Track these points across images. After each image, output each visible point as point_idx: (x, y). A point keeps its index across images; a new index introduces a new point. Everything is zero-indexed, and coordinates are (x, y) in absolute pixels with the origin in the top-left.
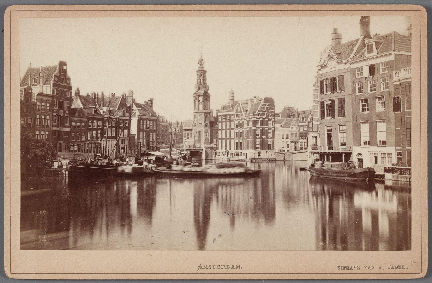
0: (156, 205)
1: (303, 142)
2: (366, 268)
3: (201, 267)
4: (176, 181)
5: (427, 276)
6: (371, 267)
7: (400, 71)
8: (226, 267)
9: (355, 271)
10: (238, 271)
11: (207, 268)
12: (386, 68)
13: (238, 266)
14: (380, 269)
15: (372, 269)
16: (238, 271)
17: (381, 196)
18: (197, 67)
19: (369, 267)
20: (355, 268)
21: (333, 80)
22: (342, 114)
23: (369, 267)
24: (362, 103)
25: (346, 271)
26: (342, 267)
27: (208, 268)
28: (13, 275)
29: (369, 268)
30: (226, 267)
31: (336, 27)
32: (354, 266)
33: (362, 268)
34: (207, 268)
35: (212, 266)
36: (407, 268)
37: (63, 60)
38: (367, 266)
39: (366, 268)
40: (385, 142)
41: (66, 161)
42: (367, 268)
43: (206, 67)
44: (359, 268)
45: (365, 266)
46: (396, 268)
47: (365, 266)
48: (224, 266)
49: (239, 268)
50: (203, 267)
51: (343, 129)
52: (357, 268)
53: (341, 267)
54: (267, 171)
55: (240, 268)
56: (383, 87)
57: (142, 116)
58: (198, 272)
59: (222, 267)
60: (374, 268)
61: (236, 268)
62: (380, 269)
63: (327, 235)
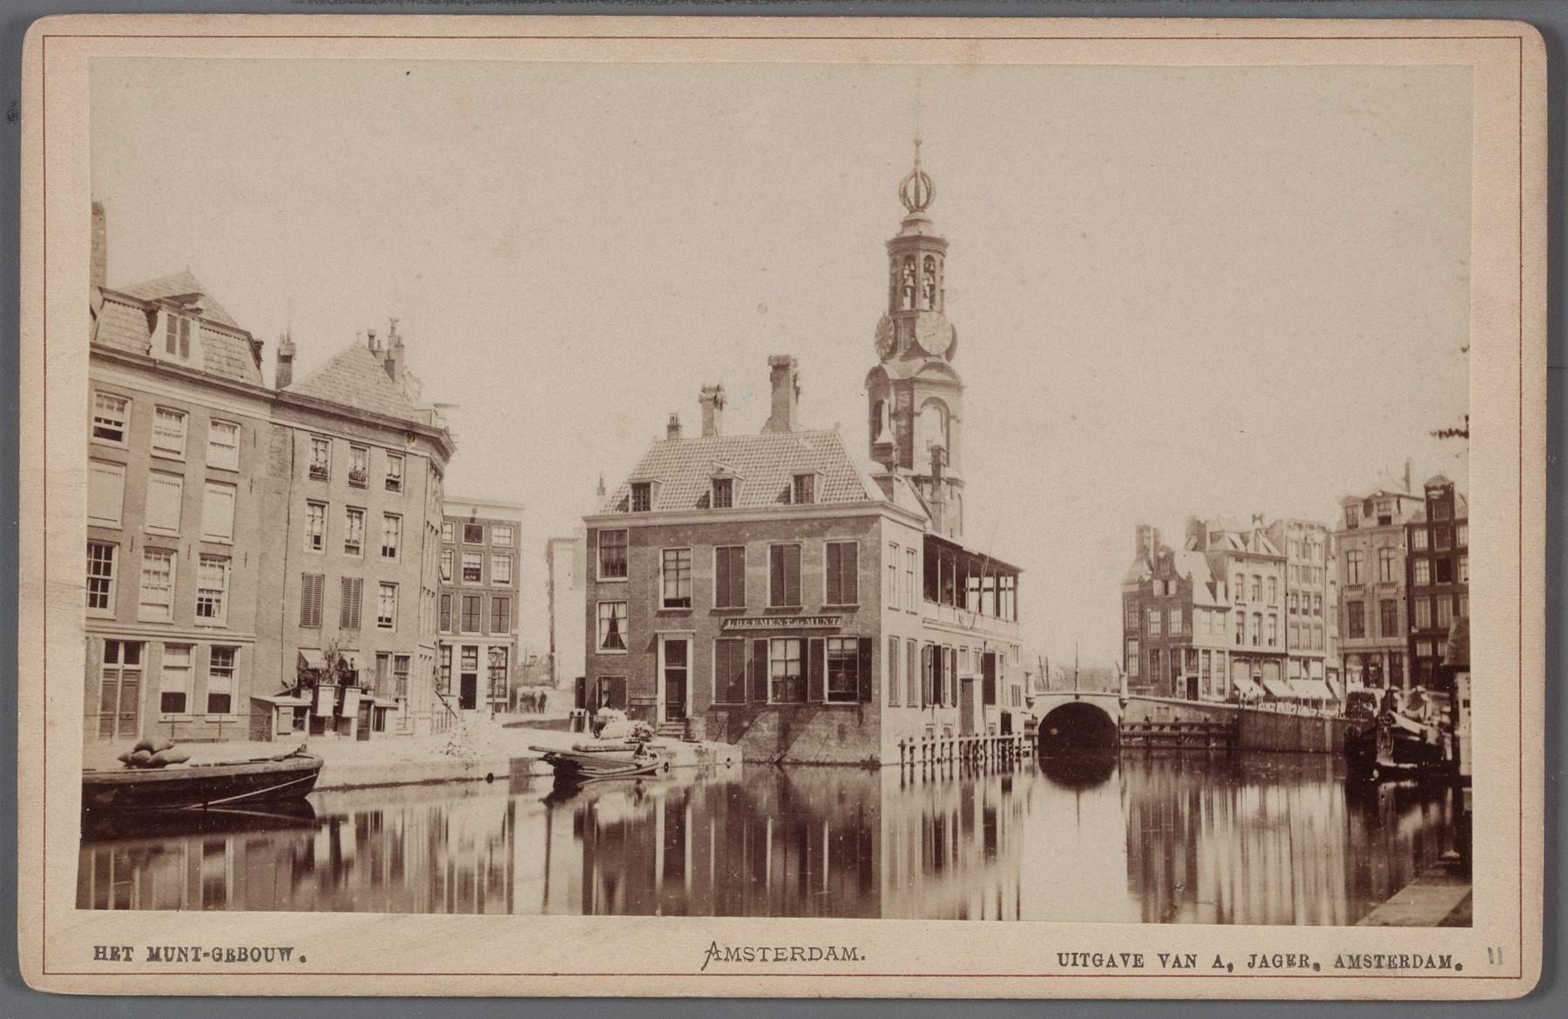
0: (1467, 598)
3: (717, 952)
6: (1183, 961)
7: (406, 367)
8: (807, 955)
11: (739, 959)
13: (849, 950)
16: (849, 967)
23: (1430, 960)
24: (106, 596)
26: (1075, 954)
30: (807, 955)
32: (1123, 955)
34: (739, 959)
35: (755, 949)
37: (778, 352)
40: (384, 554)
43: (938, 221)
45: (1161, 956)
47: (1161, 956)
48: (800, 951)
49: (855, 959)
50: (723, 955)
55: (859, 957)
56: (110, 559)
58: (704, 972)
60: (1193, 962)
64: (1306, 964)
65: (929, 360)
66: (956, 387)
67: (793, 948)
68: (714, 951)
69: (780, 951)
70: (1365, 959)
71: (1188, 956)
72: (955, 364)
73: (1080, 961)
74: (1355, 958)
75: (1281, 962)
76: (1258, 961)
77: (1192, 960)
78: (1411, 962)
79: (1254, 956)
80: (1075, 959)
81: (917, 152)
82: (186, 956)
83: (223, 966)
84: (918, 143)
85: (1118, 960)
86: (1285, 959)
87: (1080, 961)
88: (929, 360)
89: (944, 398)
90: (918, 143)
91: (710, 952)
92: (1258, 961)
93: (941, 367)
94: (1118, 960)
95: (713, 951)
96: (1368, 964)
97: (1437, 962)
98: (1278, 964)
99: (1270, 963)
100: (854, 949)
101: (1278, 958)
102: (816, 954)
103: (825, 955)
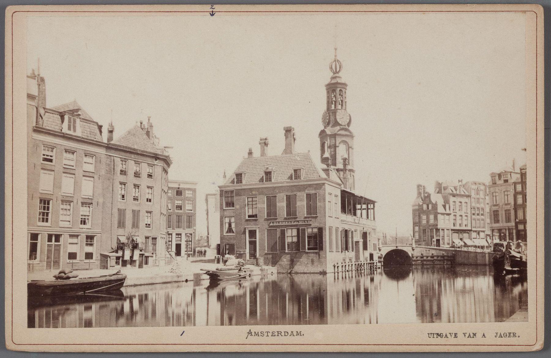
1: (40, 206)
2: (465, 336)
3: (251, 333)
4: (393, 280)
6: (472, 335)
9: (452, 340)
12: (45, 212)
18: (327, 77)
19: (470, 335)
20: (451, 336)
21: (82, 204)
22: (122, 199)
23: (470, 335)
25: (439, 340)
27: (260, 336)
31: (289, 126)
33: (460, 335)
39: (465, 336)
42: (467, 335)
43: (344, 77)
46: (505, 335)
47: (464, 334)
48: (280, 333)
50: (253, 334)
51: (519, 173)
52: (453, 335)
53: (432, 334)
55: (302, 334)
59: (278, 333)
61: (297, 335)
69: (273, 333)
71: (473, 334)
77: (475, 335)
80: (433, 335)
81: (336, 53)
84: (336, 49)
86: (508, 334)
90: (336, 49)
92: (499, 335)
93: (346, 130)
94: (449, 335)
95: (250, 333)
98: (505, 336)
100: (300, 332)
101: (505, 334)
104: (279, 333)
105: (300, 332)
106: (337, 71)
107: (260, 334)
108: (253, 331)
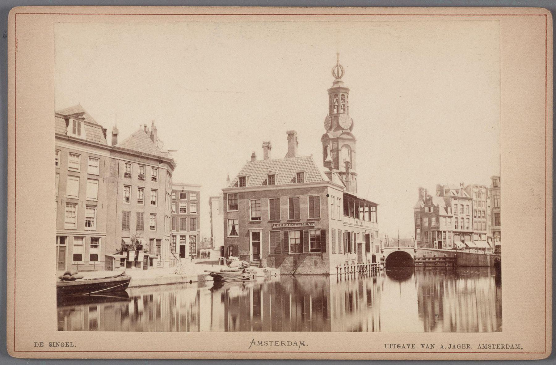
4: (395, 282)
5: (550, 358)
6: (430, 346)
8: (286, 344)
10: (303, 348)
13: (260, 343)
14: (442, 347)
15: (56, 346)
17: (251, 303)
28: (240, 354)
29: (428, 347)
30: (286, 344)
33: (46, 345)
35: (268, 341)
36: (522, 349)
38: (424, 345)
41: (447, 264)
43: (346, 82)
44: (42, 345)
48: (284, 343)
50: (257, 343)
54: (471, 279)
57: (107, 279)
59: (282, 343)
62: (442, 347)
63: (197, 321)
64: (504, 348)
65: (344, 131)
66: (353, 140)
67: (276, 342)
68: (253, 342)
70: (51, 345)
72: (353, 132)
73: (392, 347)
74: (518, 345)
75: (64, 345)
76: (452, 346)
78: (505, 347)
79: (450, 345)
82: (59, 345)
83: (397, 350)
84: (338, 54)
85: (406, 346)
86: (65, 344)
87: (392, 347)
88: (344, 131)
89: (349, 144)
90: (338, 54)
91: (252, 342)
92: (452, 346)
93: (348, 134)
94: (406, 346)
95: (253, 342)
96: (490, 347)
97: (515, 347)
99: (456, 347)
102: (290, 343)
103: (293, 344)
104: (283, 342)
105: (303, 342)
106: (340, 75)
107: (263, 343)
108: (256, 340)
